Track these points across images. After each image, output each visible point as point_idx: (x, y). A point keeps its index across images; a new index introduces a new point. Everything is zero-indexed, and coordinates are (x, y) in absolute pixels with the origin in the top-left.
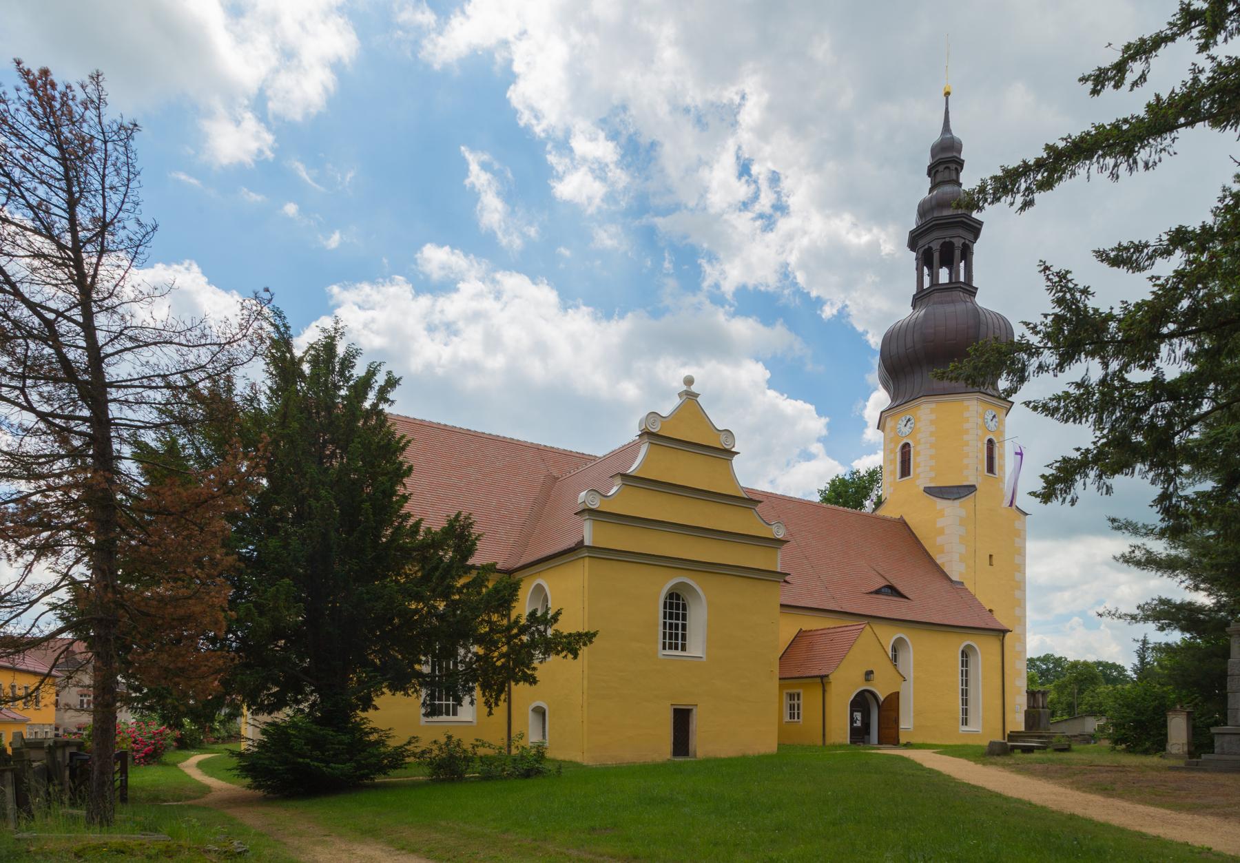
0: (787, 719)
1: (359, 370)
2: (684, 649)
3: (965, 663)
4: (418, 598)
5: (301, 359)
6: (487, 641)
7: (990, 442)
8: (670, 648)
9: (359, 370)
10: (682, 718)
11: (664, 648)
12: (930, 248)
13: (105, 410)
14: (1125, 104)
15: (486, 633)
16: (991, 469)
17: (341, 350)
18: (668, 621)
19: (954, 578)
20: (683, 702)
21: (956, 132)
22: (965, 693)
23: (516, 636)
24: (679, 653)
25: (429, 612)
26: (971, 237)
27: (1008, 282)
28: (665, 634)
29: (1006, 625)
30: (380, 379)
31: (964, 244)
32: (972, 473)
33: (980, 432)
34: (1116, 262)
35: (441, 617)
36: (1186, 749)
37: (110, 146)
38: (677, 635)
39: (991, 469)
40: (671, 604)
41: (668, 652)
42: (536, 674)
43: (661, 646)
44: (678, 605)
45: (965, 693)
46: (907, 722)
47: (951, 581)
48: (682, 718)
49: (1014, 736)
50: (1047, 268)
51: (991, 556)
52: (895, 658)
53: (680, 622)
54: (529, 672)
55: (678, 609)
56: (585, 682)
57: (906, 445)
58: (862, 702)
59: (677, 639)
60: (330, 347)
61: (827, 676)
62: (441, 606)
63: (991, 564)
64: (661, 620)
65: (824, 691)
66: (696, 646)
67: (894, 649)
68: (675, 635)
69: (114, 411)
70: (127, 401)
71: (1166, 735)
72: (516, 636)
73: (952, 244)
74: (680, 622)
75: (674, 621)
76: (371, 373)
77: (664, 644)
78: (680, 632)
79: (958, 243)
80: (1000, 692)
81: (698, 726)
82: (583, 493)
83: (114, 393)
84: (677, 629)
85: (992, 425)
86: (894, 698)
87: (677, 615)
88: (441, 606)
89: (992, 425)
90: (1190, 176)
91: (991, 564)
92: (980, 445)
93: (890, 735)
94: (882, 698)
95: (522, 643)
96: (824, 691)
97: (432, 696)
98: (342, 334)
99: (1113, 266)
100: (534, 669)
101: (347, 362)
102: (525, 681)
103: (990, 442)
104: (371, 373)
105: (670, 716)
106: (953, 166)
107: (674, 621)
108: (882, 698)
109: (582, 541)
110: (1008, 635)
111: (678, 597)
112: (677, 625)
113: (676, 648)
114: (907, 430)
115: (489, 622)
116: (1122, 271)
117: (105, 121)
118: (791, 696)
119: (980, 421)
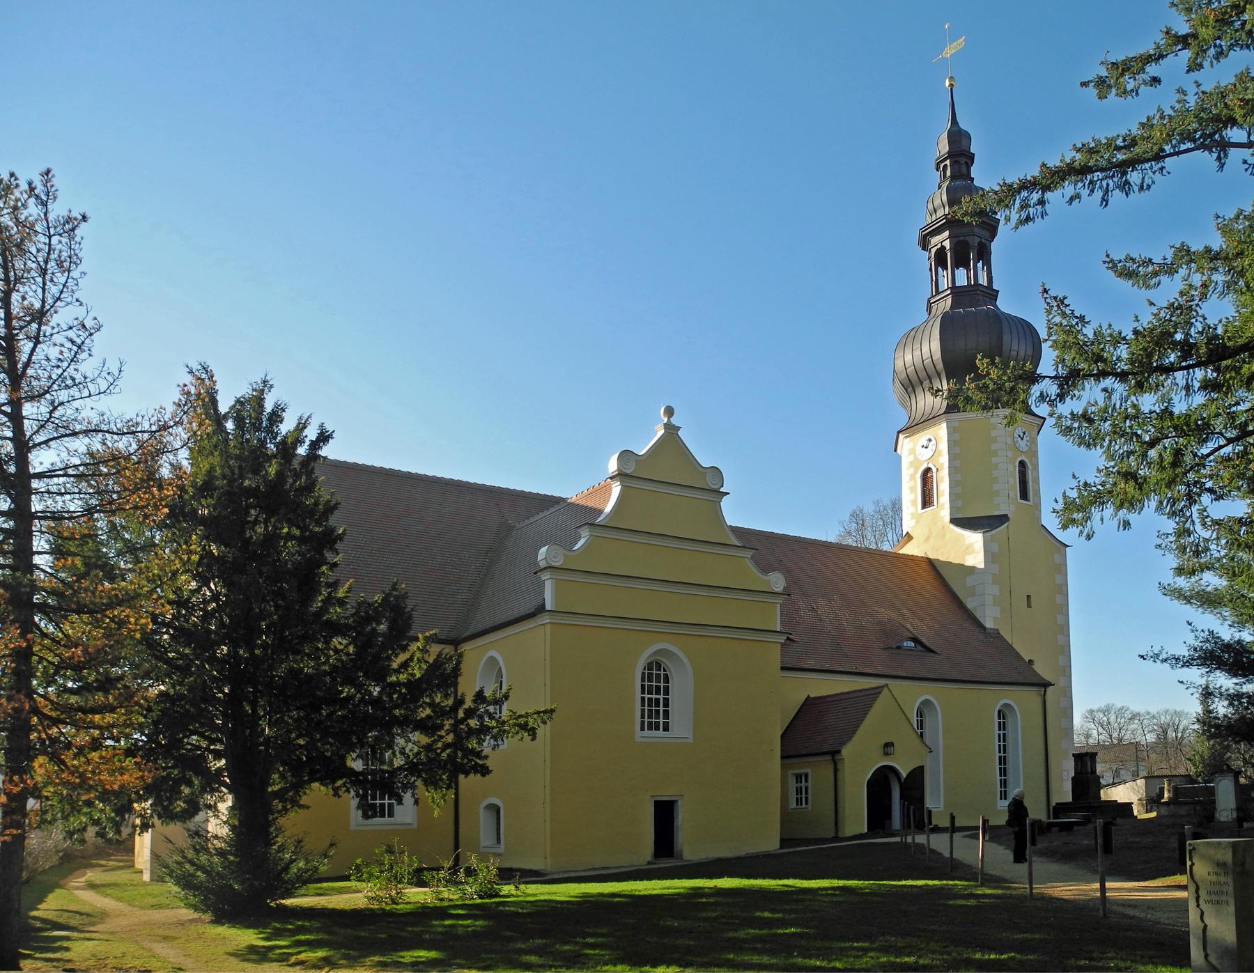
0: (793, 804)
1: (287, 427)
2: (666, 729)
3: (1002, 726)
4: (350, 681)
5: (226, 417)
6: (426, 727)
7: (1022, 464)
8: (650, 728)
9: (287, 427)
10: (665, 812)
11: (642, 729)
12: (943, 248)
13: (28, 502)
14: (1121, 118)
15: (428, 717)
16: (1024, 495)
17: (268, 407)
18: (647, 696)
19: (989, 624)
20: (665, 794)
21: (963, 125)
22: (1003, 761)
23: (463, 720)
24: (661, 732)
25: (362, 699)
26: (985, 234)
27: (1046, 270)
28: (643, 711)
29: (1048, 677)
30: (311, 434)
31: (980, 243)
32: (1005, 501)
33: (1010, 454)
34: (1128, 274)
35: (376, 702)
36: (1235, 815)
37: (55, 240)
38: (657, 712)
39: (1024, 495)
40: (650, 675)
41: (647, 732)
42: (489, 763)
43: (638, 726)
44: (658, 676)
45: (1003, 761)
46: (935, 802)
47: (984, 628)
48: (665, 812)
49: (1061, 809)
50: (1045, 291)
51: (1028, 597)
52: (921, 724)
53: (661, 697)
54: (480, 762)
55: (658, 680)
56: (548, 791)
57: (928, 470)
58: (881, 782)
59: (658, 716)
60: (259, 400)
61: (839, 752)
62: (376, 691)
63: (1029, 606)
64: (638, 695)
65: (836, 770)
66: (681, 725)
67: (920, 713)
68: (656, 712)
69: (37, 505)
70: (49, 492)
71: (1214, 802)
72: (463, 720)
73: (966, 243)
74: (661, 697)
75: (654, 696)
76: (302, 426)
77: (643, 723)
78: (661, 709)
79: (975, 241)
80: (1042, 757)
81: (683, 819)
82: (544, 549)
83: (35, 484)
84: (658, 705)
85: (1023, 444)
86: (917, 775)
87: (658, 688)
88: (376, 691)
89: (1023, 444)
90: (1193, 199)
91: (1029, 606)
92: (1011, 467)
93: (919, 819)
94: (904, 774)
95: (470, 728)
96: (836, 770)
97: (363, 798)
98: (271, 386)
99: (1120, 275)
100: (486, 757)
101: (276, 417)
102: (476, 772)
103: (1022, 464)
104: (302, 426)
105: (651, 810)
106: (963, 160)
107: (654, 696)
108: (904, 774)
109: (544, 605)
110: (1050, 689)
111: (659, 666)
112: (658, 700)
113: (657, 728)
114: (928, 453)
115: (432, 705)
116: (1127, 284)
117: (51, 217)
118: (798, 778)
119: (1009, 441)
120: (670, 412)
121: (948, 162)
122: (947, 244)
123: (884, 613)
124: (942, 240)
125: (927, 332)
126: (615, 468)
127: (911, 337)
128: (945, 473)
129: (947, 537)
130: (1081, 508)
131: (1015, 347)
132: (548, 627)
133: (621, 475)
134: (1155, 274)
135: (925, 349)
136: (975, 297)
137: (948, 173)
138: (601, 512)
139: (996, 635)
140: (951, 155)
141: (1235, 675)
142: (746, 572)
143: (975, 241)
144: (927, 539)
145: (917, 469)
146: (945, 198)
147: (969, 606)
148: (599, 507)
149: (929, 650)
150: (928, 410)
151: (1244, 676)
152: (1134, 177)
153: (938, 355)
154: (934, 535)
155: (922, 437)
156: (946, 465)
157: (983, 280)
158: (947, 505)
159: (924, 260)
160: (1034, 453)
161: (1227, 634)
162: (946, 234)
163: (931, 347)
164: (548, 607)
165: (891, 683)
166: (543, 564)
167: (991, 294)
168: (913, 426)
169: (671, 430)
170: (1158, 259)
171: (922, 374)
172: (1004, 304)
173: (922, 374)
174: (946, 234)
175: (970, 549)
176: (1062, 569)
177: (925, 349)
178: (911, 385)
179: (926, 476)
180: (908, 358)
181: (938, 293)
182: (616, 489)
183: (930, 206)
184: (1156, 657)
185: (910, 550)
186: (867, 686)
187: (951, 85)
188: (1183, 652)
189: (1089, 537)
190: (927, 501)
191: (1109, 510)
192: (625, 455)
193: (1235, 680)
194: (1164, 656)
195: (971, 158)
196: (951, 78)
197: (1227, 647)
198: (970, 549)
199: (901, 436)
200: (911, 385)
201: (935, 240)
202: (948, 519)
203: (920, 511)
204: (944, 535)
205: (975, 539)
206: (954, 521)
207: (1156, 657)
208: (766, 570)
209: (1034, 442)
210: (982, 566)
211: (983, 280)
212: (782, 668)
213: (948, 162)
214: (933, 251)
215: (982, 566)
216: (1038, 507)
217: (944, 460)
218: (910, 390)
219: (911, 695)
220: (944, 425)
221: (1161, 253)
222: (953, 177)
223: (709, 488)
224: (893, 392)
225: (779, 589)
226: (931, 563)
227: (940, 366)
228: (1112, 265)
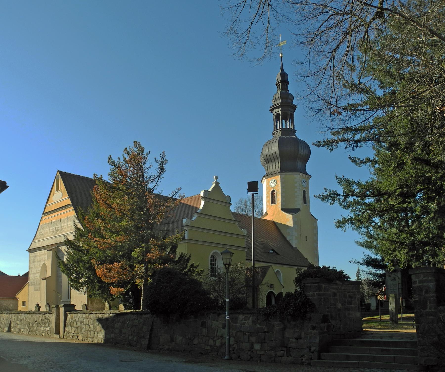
7: (304, 191)
12: (279, 114)
16: (305, 202)
19: (294, 246)
32: (299, 204)
38: (213, 271)
39: (305, 202)
47: (292, 247)
57: (273, 191)
59: (213, 272)
63: (306, 240)
74: (214, 266)
89: (304, 184)
99: (352, 161)
109: (185, 237)
114: (273, 185)
116: (354, 164)
120: (216, 178)
121: (280, 84)
122: (280, 113)
123: (263, 240)
124: (278, 111)
125: (274, 143)
126: (203, 195)
127: (268, 143)
128: (280, 192)
129: (280, 215)
130: (343, 224)
131: (302, 151)
132: (186, 244)
133: (205, 198)
134: (361, 163)
135: (273, 148)
136: (289, 132)
137: (280, 87)
138: (198, 209)
139: (296, 249)
140: (281, 81)
141: (374, 268)
142: (235, 228)
143: (289, 113)
144: (273, 215)
145: (269, 191)
146: (279, 96)
147: (288, 239)
148: (196, 206)
149: (278, 254)
150: (273, 170)
151: (377, 269)
152: (359, 144)
153: (277, 152)
154: (271, 210)
155: (272, 180)
156: (280, 190)
157: (292, 127)
158: (280, 204)
159: (271, 117)
160: (307, 188)
161: (373, 256)
162: (280, 109)
163: (275, 148)
164: (186, 237)
165: (273, 265)
166: (184, 225)
167: (294, 131)
168: (268, 175)
169: (217, 184)
170: (362, 159)
171: (272, 158)
172: (299, 135)
173: (272, 158)
174: (280, 109)
175: (288, 220)
176: (316, 228)
177: (273, 148)
178: (268, 160)
179: (273, 193)
180: (267, 150)
181: (277, 129)
182: (203, 203)
183: (274, 98)
184: (353, 262)
185: (267, 218)
186: (263, 266)
187: (282, 56)
188: (361, 261)
189: (345, 231)
190: (273, 201)
191: (350, 225)
192: (206, 192)
193: (374, 270)
194: (356, 262)
195: (288, 83)
196: (281, 54)
197: (373, 260)
198: (288, 220)
199: (264, 178)
200: (268, 160)
201: (276, 110)
202: (280, 209)
203: (271, 205)
204: (279, 214)
205: (290, 217)
206: (283, 210)
207: (353, 262)
208: (242, 227)
209: (308, 184)
210: (292, 226)
211: (292, 127)
212: (247, 259)
213: (280, 84)
214: (275, 114)
215: (292, 226)
216: (309, 207)
217: (279, 188)
218: (267, 162)
219: (276, 268)
220: (279, 176)
221: (363, 158)
222: (282, 89)
223: (227, 201)
224: (259, 161)
225: (245, 234)
226: (275, 223)
227: (278, 156)
228: (350, 158)
